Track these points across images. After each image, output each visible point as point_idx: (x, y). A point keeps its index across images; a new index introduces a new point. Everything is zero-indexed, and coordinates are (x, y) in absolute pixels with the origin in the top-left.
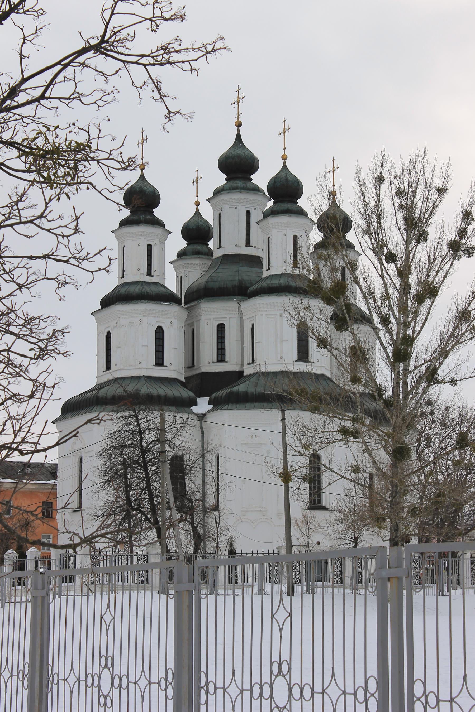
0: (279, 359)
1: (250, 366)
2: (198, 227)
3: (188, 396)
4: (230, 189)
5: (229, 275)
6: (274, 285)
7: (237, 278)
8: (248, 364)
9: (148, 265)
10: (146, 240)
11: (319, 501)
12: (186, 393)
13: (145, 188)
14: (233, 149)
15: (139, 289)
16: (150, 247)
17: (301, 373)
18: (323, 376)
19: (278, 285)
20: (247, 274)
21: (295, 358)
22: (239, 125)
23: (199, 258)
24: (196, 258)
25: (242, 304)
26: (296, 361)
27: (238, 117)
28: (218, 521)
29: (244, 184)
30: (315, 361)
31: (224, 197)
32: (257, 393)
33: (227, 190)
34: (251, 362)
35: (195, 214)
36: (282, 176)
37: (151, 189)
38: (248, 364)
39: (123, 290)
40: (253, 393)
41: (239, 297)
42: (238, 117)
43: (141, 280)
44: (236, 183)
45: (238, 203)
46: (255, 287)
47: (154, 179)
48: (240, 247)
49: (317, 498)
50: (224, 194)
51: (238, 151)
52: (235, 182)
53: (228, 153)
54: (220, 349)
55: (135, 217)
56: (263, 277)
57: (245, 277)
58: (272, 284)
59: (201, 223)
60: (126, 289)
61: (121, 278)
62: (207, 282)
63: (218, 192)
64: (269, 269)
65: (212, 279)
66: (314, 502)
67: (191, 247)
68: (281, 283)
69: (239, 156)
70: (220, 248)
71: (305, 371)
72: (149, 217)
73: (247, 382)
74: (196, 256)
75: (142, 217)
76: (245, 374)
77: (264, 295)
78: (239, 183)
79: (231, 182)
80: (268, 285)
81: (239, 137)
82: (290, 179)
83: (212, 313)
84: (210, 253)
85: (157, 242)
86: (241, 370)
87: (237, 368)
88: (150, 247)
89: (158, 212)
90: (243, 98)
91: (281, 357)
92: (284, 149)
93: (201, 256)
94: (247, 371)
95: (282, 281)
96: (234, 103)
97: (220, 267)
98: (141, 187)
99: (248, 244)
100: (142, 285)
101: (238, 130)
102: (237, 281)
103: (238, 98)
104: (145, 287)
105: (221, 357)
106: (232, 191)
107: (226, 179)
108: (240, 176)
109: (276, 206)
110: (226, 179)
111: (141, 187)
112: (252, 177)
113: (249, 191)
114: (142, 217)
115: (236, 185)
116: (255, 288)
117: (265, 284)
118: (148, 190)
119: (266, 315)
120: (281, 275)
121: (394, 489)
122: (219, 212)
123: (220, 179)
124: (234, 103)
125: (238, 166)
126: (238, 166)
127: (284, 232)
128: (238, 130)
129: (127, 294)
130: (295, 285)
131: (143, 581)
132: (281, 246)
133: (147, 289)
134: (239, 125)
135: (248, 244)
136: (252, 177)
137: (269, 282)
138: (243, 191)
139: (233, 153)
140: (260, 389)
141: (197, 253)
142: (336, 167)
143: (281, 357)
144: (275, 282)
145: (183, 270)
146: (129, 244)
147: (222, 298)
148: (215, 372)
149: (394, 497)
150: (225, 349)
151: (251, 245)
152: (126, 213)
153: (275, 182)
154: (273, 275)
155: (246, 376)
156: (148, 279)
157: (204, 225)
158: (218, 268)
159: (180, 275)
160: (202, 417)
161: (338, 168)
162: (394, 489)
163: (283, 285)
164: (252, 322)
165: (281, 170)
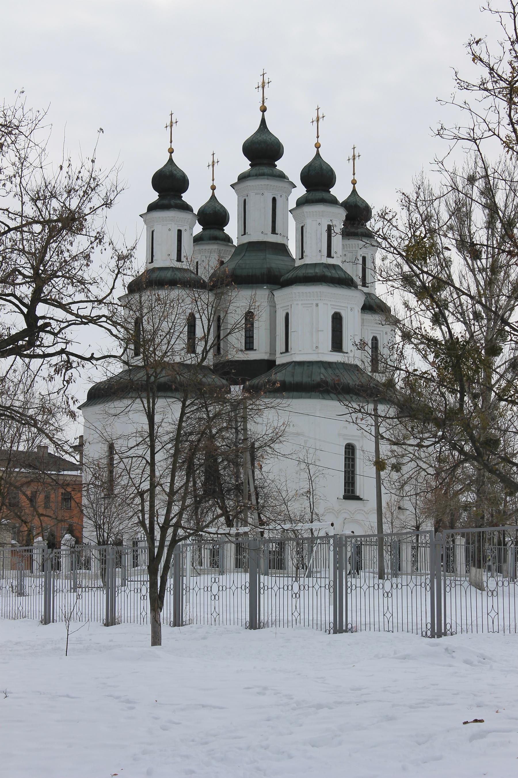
0: (314, 348)
1: (283, 355)
2: (215, 211)
3: (221, 383)
4: (256, 175)
5: (255, 263)
6: (310, 275)
7: (266, 266)
8: (281, 353)
9: (178, 251)
10: (176, 226)
11: (353, 491)
12: (218, 380)
13: (175, 172)
14: (259, 134)
15: (171, 275)
16: (180, 232)
17: (335, 363)
18: (356, 366)
19: (314, 274)
20: (275, 262)
21: (330, 348)
22: (264, 110)
23: (217, 243)
24: (214, 243)
25: (276, 293)
26: (331, 351)
27: (263, 101)
28: (312, 507)
29: (271, 171)
30: (349, 352)
31: (250, 183)
32: (295, 382)
33: (253, 176)
34: (284, 351)
35: (211, 198)
36: (316, 165)
37: (181, 174)
38: (281, 353)
39: (155, 275)
40: (290, 383)
41: (268, 285)
42: (263, 101)
43: (171, 266)
44: (262, 170)
45: (262, 191)
46: (290, 275)
47: (182, 163)
48: (267, 234)
49: (351, 488)
50: (250, 180)
51: (264, 137)
52: (261, 168)
53: (254, 138)
54: (248, 337)
55: (165, 202)
56: (296, 265)
57: (273, 265)
58: (308, 273)
59: (218, 208)
60: (156, 274)
61: (150, 263)
62: (234, 269)
63: (243, 178)
64: (302, 258)
65: (239, 266)
66: (349, 492)
67: (208, 232)
68: (317, 273)
69: (265, 142)
70: (245, 234)
71: (339, 361)
72: (179, 202)
73: (284, 371)
74: (213, 241)
75: (173, 202)
76: (277, 363)
77: (300, 284)
78: (266, 170)
79: (257, 168)
80: (303, 274)
81: (263, 122)
82: (324, 167)
83: (240, 300)
84: (227, 239)
85: (187, 227)
86: (271, 358)
87: (266, 357)
88: (180, 232)
89: (186, 197)
90: (269, 83)
91: (317, 347)
92: (318, 137)
93: (218, 242)
94: (280, 360)
95: (317, 270)
96: (258, 87)
97: (246, 255)
98: (171, 171)
99: (274, 231)
100: (173, 271)
101: (263, 115)
102: (266, 268)
103: (263, 82)
104: (177, 273)
105: (249, 345)
106: (259, 177)
107: (250, 165)
108: (265, 162)
109: (311, 194)
110: (250, 165)
111: (171, 171)
112: (276, 163)
113: (275, 178)
114: (172, 203)
115: (262, 171)
116: (289, 277)
117: (301, 273)
118: (178, 175)
119: (302, 304)
120: (315, 265)
121: (482, 478)
122: (244, 198)
123: (244, 165)
124: (258, 87)
125: (263, 152)
126: (263, 152)
127: (319, 221)
128: (263, 115)
129: (159, 280)
130: (330, 274)
131: (216, 564)
132: (305, 235)
133: (179, 275)
134: (264, 110)
135: (274, 231)
136: (276, 163)
137: (304, 272)
138: (269, 177)
139: (260, 139)
140: (298, 379)
141: (215, 239)
142: (357, 155)
143: (317, 347)
144: (311, 272)
145: (200, 255)
146: (158, 229)
147: (250, 285)
148: (243, 361)
149: (482, 486)
150: (253, 337)
151: (276, 232)
152: (154, 196)
153: (309, 171)
154: (307, 264)
155: (279, 365)
156: (178, 265)
157: (221, 210)
158: (244, 255)
159: (196, 260)
160: (236, 405)
161: (359, 156)
162: (482, 478)
163: (319, 274)
164: (287, 311)
165: (315, 159)
